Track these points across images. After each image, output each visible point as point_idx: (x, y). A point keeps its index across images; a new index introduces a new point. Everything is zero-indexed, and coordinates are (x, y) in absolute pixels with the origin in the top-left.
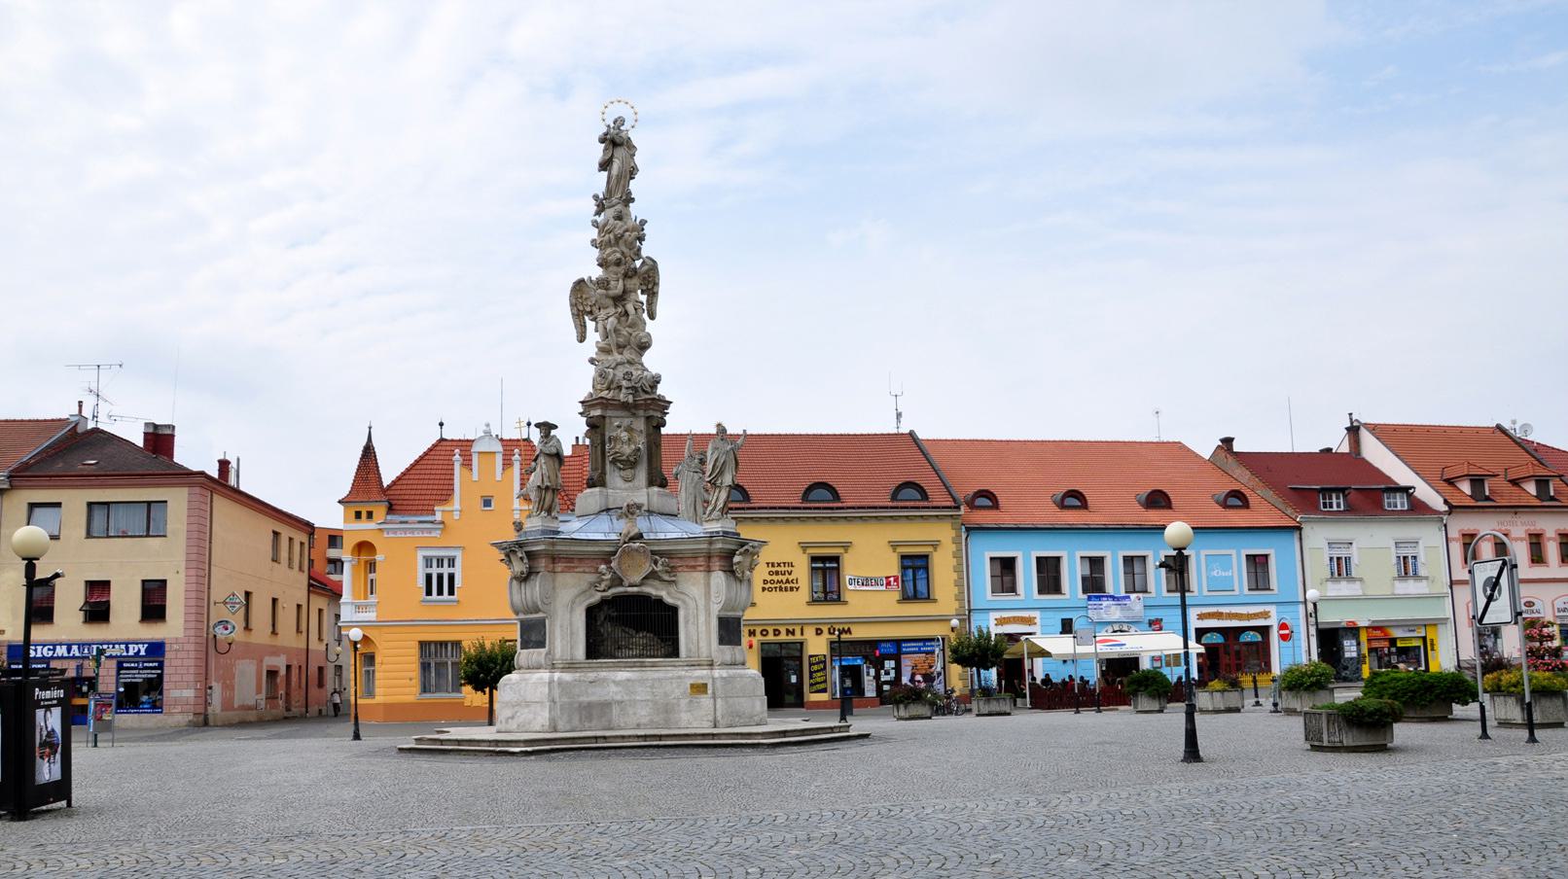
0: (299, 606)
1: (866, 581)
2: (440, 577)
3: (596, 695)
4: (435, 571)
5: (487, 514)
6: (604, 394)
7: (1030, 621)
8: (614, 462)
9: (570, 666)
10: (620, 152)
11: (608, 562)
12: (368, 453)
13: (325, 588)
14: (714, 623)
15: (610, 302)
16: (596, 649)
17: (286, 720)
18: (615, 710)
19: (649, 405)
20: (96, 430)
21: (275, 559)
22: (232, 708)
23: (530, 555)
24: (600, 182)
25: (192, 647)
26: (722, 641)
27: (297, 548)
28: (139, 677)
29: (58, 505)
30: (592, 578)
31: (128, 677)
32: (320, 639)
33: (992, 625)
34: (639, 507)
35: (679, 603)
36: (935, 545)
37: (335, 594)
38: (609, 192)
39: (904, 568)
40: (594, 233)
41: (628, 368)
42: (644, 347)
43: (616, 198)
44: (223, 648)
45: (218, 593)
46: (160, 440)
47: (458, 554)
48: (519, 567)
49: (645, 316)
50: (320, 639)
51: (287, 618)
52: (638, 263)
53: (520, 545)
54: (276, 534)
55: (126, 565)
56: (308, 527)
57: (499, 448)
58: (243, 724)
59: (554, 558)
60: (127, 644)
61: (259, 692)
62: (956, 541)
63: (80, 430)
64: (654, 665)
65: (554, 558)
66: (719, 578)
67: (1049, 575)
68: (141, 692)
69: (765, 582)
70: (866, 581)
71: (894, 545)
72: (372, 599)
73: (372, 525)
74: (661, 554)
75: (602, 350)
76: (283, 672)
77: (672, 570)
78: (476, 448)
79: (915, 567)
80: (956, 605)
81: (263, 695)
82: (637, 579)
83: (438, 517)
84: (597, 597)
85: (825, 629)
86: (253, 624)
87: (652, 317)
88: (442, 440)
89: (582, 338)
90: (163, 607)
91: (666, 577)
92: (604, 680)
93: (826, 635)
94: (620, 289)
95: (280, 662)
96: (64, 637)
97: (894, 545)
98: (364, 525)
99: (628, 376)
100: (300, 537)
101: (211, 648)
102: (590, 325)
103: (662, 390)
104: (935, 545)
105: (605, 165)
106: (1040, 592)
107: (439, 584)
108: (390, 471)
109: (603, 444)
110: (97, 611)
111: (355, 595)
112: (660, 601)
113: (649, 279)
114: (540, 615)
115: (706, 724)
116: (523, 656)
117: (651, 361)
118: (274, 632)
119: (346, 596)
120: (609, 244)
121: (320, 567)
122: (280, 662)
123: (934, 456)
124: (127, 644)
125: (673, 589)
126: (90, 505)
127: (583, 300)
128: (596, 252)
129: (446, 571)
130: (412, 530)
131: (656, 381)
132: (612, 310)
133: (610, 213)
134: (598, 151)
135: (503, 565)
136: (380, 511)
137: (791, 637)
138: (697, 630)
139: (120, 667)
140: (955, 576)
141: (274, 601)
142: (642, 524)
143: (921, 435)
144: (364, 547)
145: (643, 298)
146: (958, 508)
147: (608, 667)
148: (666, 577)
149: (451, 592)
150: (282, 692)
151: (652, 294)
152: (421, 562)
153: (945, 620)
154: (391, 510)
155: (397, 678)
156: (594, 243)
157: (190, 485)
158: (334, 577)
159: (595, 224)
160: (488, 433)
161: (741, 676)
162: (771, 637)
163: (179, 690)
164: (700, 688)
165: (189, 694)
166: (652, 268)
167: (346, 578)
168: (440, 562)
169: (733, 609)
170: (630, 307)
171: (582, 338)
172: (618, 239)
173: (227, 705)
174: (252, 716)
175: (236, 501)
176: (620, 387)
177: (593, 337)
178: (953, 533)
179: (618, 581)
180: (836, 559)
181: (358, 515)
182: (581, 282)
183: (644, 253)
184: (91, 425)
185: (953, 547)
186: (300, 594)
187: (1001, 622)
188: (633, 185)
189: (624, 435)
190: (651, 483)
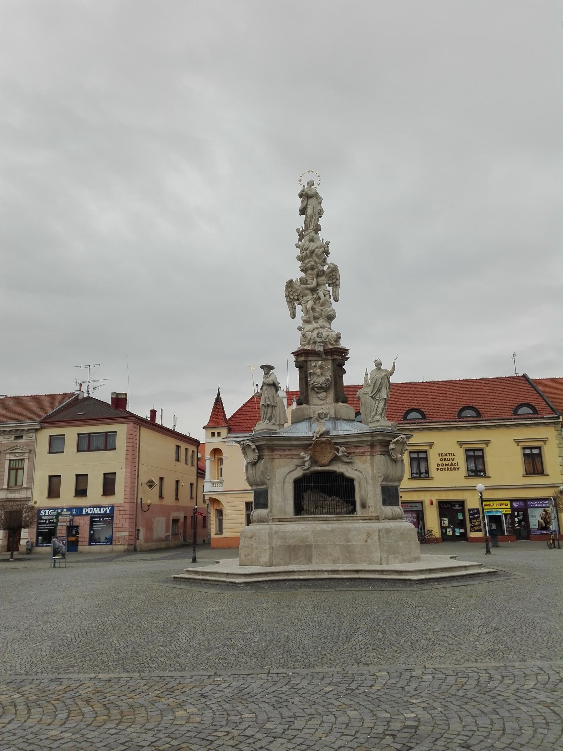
0: (192, 485)
8: (313, 389)
10: (312, 201)
12: (218, 402)
14: (379, 491)
15: (309, 292)
17: (176, 547)
20: (89, 398)
22: (152, 541)
25: (128, 508)
27: (190, 453)
30: (297, 461)
36: (545, 441)
40: (298, 252)
42: (330, 318)
44: (146, 508)
45: (143, 479)
46: (119, 401)
48: (253, 456)
49: (332, 300)
51: (185, 491)
52: (326, 268)
54: (178, 447)
55: (96, 465)
61: (167, 531)
65: (272, 449)
66: (380, 459)
69: (438, 465)
71: (518, 442)
73: (220, 439)
76: (182, 519)
81: (170, 534)
82: (325, 461)
84: (299, 473)
86: (165, 494)
87: (336, 300)
89: (293, 316)
90: (86, 489)
91: (346, 460)
94: (316, 281)
97: (518, 442)
98: (216, 439)
99: (319, 335)
100: (191, 448)
101: (139, 509)
102: (299, 308)
103: (343, 344)
104: (545, 441)
105: (303, 211)
109: (306, 378)
110: (81, 491)
112: (342, 475)
113: (333, 277)
114: (265, 486)
117: (336, 326)
118: (177, 499)
120: (306, 257)
122: (180, 515)
128: (300, 263)
131: (338, 338)
132: (310, 297)
134: (298, 203)
136: (224, 432)
138: (368, 490)
141: (177, 482)
143: (532, 377)
144: (216, 452)
145: (330, 289)
148: (346, 460)
150: (181, 531)
151: (335, 284)
154: (230, 431)
157: (128, 422)
159: (297, 246)
163: (123, 532)
165: (126, 534)
166: (334, 270)
170: (321, 294)
171: (293, 316)
172: (312, 252)
174: (163, 545)
176: (315, 343)
178: (556, 433)
181: (213, 434)
182: (291, 281)
183: (329, 260)
184: (86, 395)
188: (321, 221)
189: (319, 371)
190: (337, 400)
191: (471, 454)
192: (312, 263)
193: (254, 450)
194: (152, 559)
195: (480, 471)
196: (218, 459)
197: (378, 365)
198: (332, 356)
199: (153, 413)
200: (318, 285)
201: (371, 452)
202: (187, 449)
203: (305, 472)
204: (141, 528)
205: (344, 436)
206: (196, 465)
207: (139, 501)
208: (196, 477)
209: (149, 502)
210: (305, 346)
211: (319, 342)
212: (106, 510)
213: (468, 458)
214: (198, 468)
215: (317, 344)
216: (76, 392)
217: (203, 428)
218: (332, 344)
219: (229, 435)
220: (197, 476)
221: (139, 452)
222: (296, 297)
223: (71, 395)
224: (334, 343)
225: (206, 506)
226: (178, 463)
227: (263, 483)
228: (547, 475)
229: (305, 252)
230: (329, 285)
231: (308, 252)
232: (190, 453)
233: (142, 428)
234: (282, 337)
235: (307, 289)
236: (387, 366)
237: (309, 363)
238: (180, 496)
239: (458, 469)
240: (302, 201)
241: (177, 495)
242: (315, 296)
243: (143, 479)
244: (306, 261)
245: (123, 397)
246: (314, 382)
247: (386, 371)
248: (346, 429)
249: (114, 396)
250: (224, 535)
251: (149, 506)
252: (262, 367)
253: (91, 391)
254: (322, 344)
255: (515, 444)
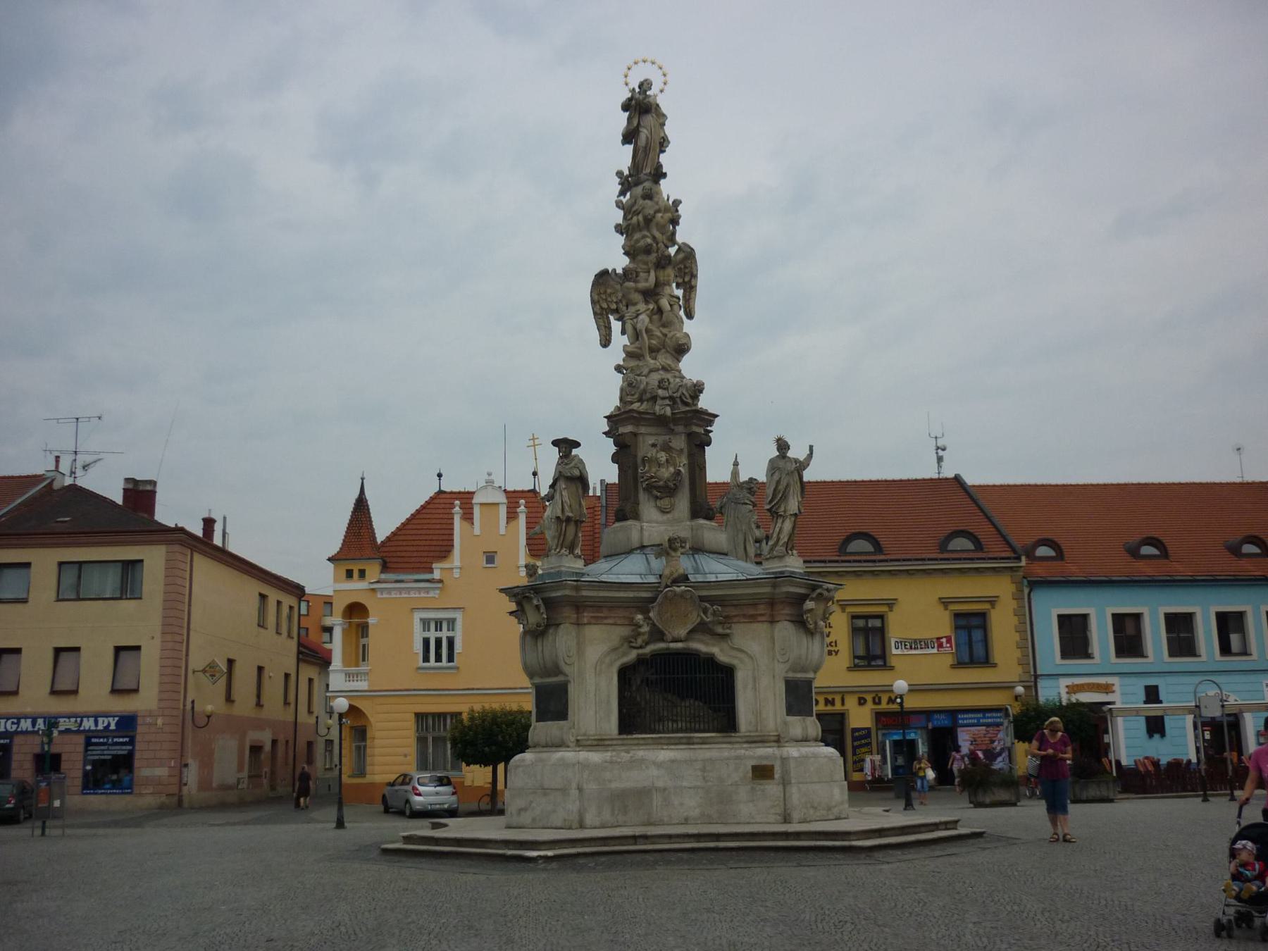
0: (287, 676)
1: (915, 644)
2: (438, 642)
3: (632, 780)
4: (432, 635)
5: (489, 558)
6: (636, 406)
7: (1107, 689)
8: (649, 489)
9: (599, 743)
10: (649, 120)
11: (645, 612)
12: (361, 506)
13: (313, 656)
14: (781, 687)
16: (632, 721)
17: (258, 802)
18: (657, 800)
19: (688, 421)
20: (74, 488)
21: (262, 625)
23: (550, 604)
24: (624, 157)
26: (1156, 687)
27: (285, 610)
28: (106, 753)
29: (27, 565)
31: (97, 753)
32: (310, 712)
33: (1054, 692)
34: (683, 541)
35: (735, 662)
36: (992, 601)
37: (324, 662)
38: (636, 166)
39: (957, 628)
40: (618, 216)
41: (662, 374)
42: (681, 349)
43: (643, 176)
45: (198, 660)
46: (140, 496)
47: (458, 616)
49: (682, 313)
50: (310, 712)
51: (273, 689)
52: (672, 251)
53: (535, 589)
54: (263, 597)
56: (296, 590)
57: (502, 499)
58: (223, 806)
59: (579, 606)
60: (19, 719)
61: (240, 769)
62: (1018, 597)
63: (56, 486)
64: (704, 742)
66: (785, 630)
67: (1128, 638)
68: (112, 769)
70: (915, 644)
71: (945, 603)
72: (363, 668)
74: (712, 600)
75: (630, 355)
76: (268, 747)
77: (727, 621)
78: (477, 499)
79: (971, 628)
80: (1020, 670)
81: (245, 774)
82: (682, 632)
83: (437, 575)
84: (632, 656)
85: (869, 698)
86: (236, 695)
87: (690, 316)
88: (440, 492)
89: (606, 342)
91: (719, 630)
92: (642, 761)
93: (870, 705)
94: (649, 280)
95: (265, 737)
96: (28, 710)
97: (945, 603)
98: (357, 585)
100: (288, 600)
102: (616, 326)
103: (704, 403)
104: (992, 601)
105: (629, 137)
106: (1171, 655)
107: (440, 650)
108: (384, 525)
111: (346, 662)
112: (711, 661)
113: (685, 267)
115: (772, 818)
116: (539, 731)
117: (690, 368)
118: (259, 705)
119: (337, 662)
121: (314, 636)
122: (265, 737)
123: (982, 502)
124: (96, 718)
125: (725, 645)
126: (61, 564)
127: (609, 295)
128: (621, 240)
129: (444, 634)
130: (409, 590)
131: (697, 389)
132: (642, 307)
133: (639, 190)
135: (513, 620)
136: (373, 570)
137: (829, 708)
138: (759, 698)
139: (88, 743)
140: (1017, 637)
141: (260, 669)
142: (684, 564)
143: (971, 479)
144: (356, 610)
145: (679, 293)
146: (1019, 559)
147: (646, 743)
149: (451, 658)
150: (266, 769)
151: (689, 288)
152: (417, 626)
153: (1009, 687)
154: (385, 568)
155: (392, 750)
156: (619, 229)
157: (167, 542)
158: (327, 646)
159: (619, 205)
160: (490, 483)
161: (815, 756)
162: (884, 706)
163: (152, 769)
164: (762, 772)
166: (688, 255)
167: (337, 646)
168: (439, 625)
169: (804, 670)
170: (664, 303)
171: (606, 342)
173: (204, 785)
175: (220, 561)
176: (654, 399)
177: (620, 341)
179: (657, 634)
180: (983, 616)
181: (349, 574)
183: (680, 238)
184: (68, 481)
185: (1014, 604)
186: (290, 663)
187: (1073, 689)
189: (663, 456)
191: (861, 623)
192: (649, 241)
193: (537, 607)
194: (228, 824)
195: (875, 658)
196: (358, 625)
197: (782, 446)
198: (686, 426)
199: (209, 523)
200: (657, 284)
201: (772, 616)
202: (279, 603)
203: (641, 651)
204: (190, 761)
205: (719, 584)
206: (295, 634)
207: (189, 706)
208: (294, 661)
209: (209, 708)
210: (632, 403)
211: (664, 398)
212: (109, 724)
213: (855, 631)
214: (300, 644)
215: (659, 402)
216: (49, 474)
217: (329, 559)
218: (686, 404)
219: (383, 576)
220: (298, 660)
221: (190, 605)
222: (614, 306)
223: (36, 479)
224: (690, 401)
225: (313, 721)
226: (262, 630)
227: (557, 671)
228: (995, 665)
229: (635, 219)
230: (678, 286)
231: (640, 217)
232: (285, 610)
233: (197, 557)
234: (584, 382)
235: (637, 290)
236: (797, 452)
237: (641, 438)
238: (264, 700)
239: (837, 653)
240: (629, 119)
241: (259, 696)
242: (651, 306)
243: (198, 660)
244: (637, 236)
245: (149, 488)
246: (652, 477)
247: (796, 461)
248: (719, 570)
249: (130, 486)
250: (369, 779)
251: (209, 717)
252: (555, 443)
253: (79, 472)
254: (667, 402)
255: (941, 608)
